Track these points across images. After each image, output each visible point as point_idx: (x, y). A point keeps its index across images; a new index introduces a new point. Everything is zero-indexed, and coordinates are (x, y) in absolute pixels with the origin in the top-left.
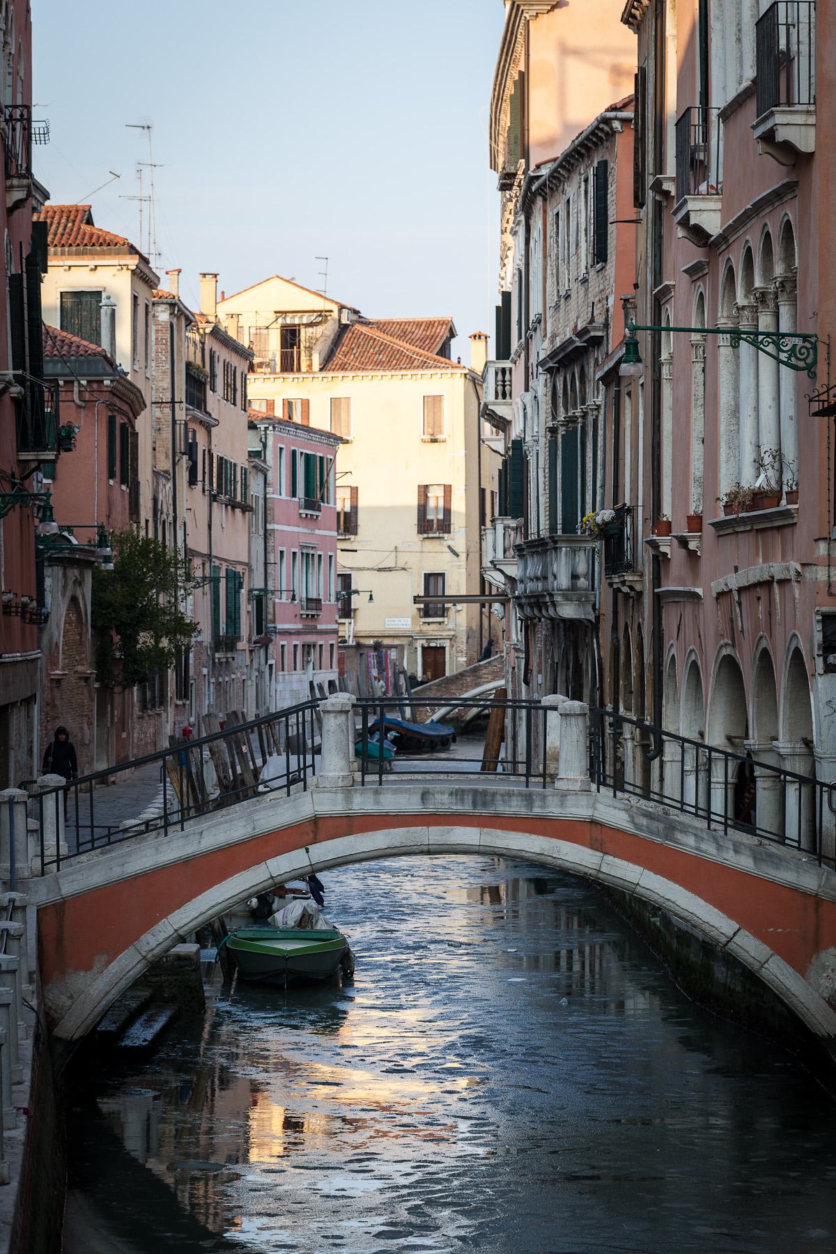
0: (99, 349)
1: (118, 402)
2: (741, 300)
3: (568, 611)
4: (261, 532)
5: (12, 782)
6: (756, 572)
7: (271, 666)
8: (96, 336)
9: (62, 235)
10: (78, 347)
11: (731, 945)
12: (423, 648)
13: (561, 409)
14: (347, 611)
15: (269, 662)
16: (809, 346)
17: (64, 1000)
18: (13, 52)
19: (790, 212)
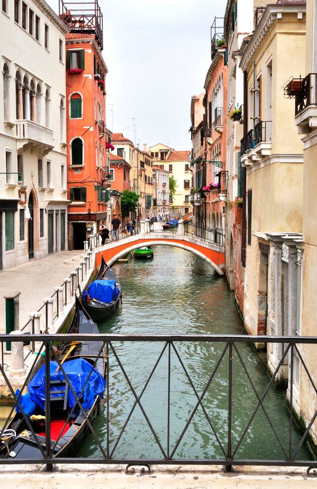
2: (215, 155)
19: (220, 141)
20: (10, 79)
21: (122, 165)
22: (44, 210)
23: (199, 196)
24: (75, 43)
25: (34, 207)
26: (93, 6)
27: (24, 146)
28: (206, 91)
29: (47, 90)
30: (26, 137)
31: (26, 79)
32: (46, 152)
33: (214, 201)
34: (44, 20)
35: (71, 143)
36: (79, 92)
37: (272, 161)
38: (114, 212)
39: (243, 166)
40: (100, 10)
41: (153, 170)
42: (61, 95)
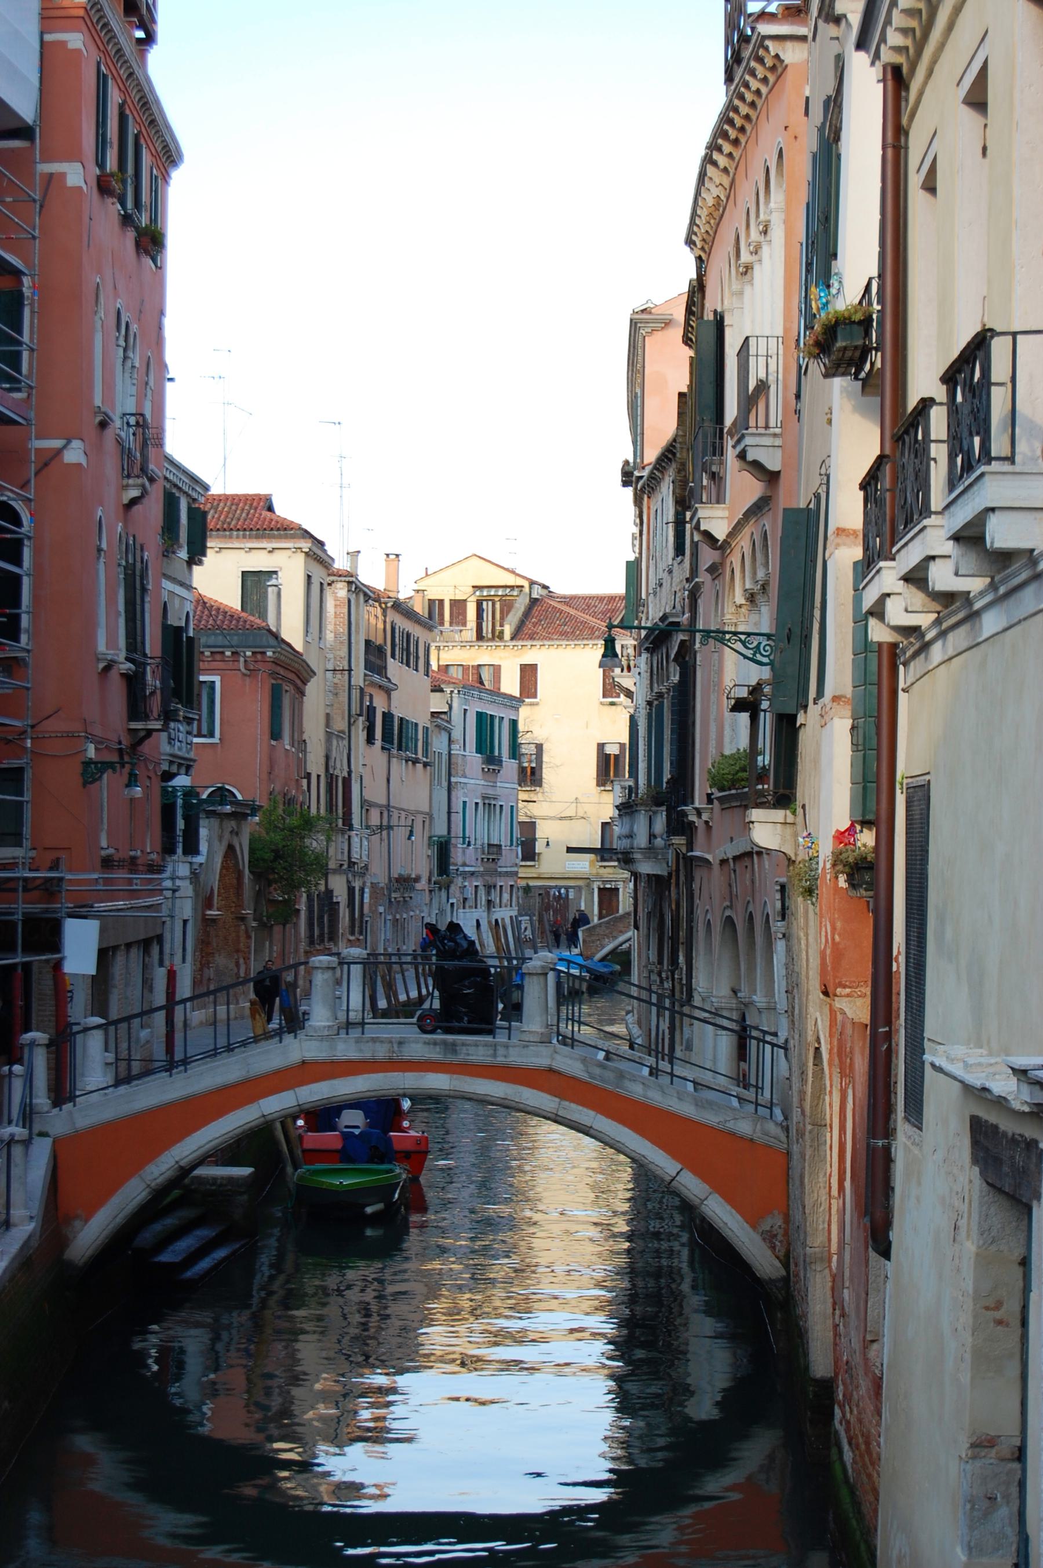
0: (264, 624)
1: (282, 671)
4: (445, 784)
5: (34, 1026)
7: (452, 904)
8: (263, 615)
9: (245, 520)
10: (245, 621)
11: (674, 1183)
12: (600, 889)
13: (656, 685)
15: (451, 901)
16: (773, 644)
18: (137, 365)
23: (660, 824)
28: (699, 259)
38: (208, 904)
39: (878, 633)
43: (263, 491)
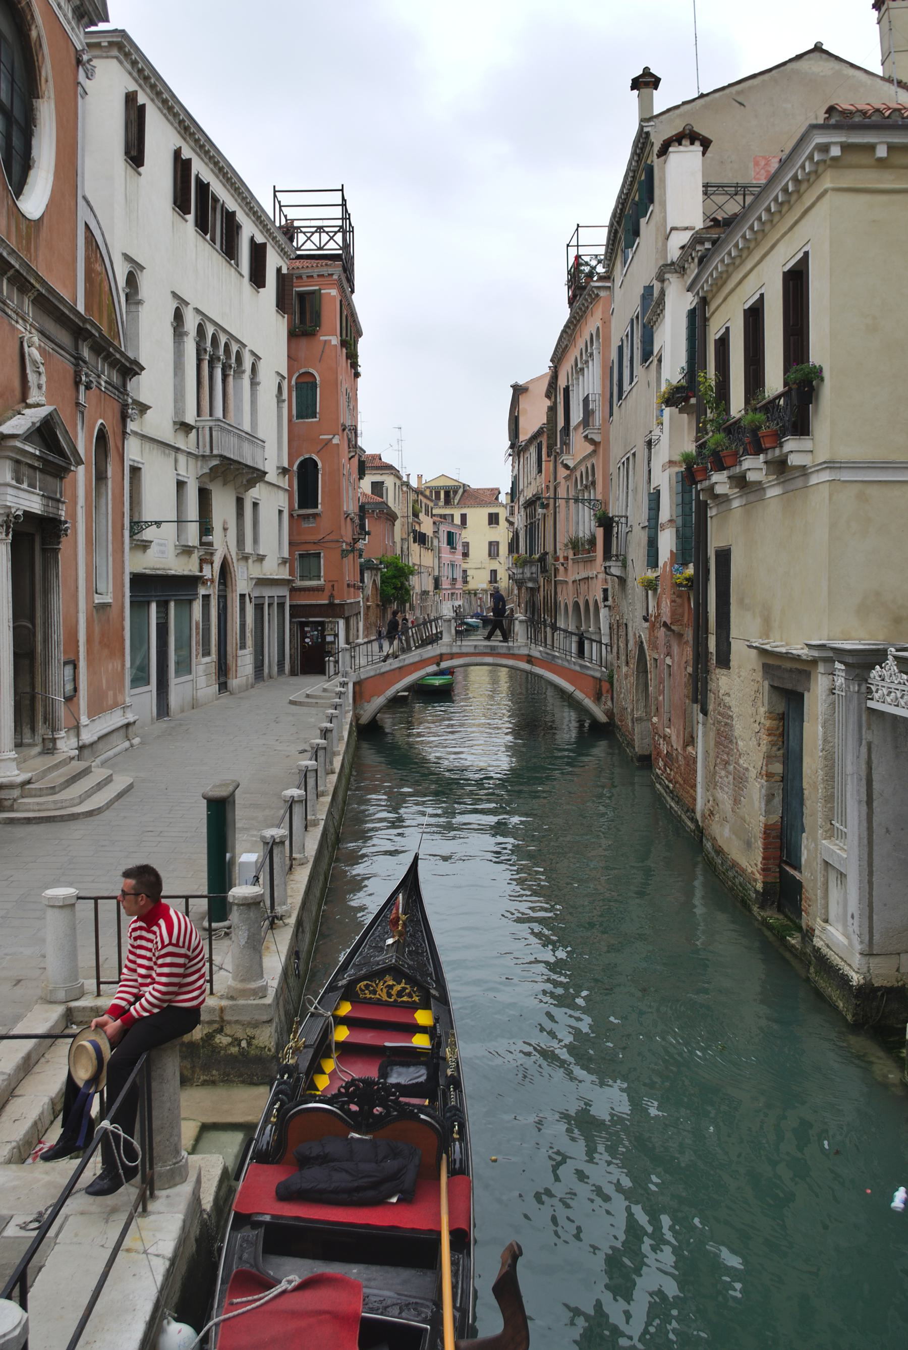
3: (530, 585)
6: (583, 575)
14: (465, 582)
17: (362, 712)
19: (594, 461)
20: (185, 339)
21: (381, 511)
22: (247, 597)
24: (304, 277)
25: (229, 590)
26: (338, 212)
27: (211, 469)
29: (253, 364)
30: (215, 452)
31: (215, 339)
32: (251, 484)
33: (578, 577)
34: (248, 230)
35: (295, 467)
36: (311, 370)
37: (814, 480)
38: (368, 600)
40: (349, 219)
41: (434, 523)
42: (278, 373)
43: (378, 453)
